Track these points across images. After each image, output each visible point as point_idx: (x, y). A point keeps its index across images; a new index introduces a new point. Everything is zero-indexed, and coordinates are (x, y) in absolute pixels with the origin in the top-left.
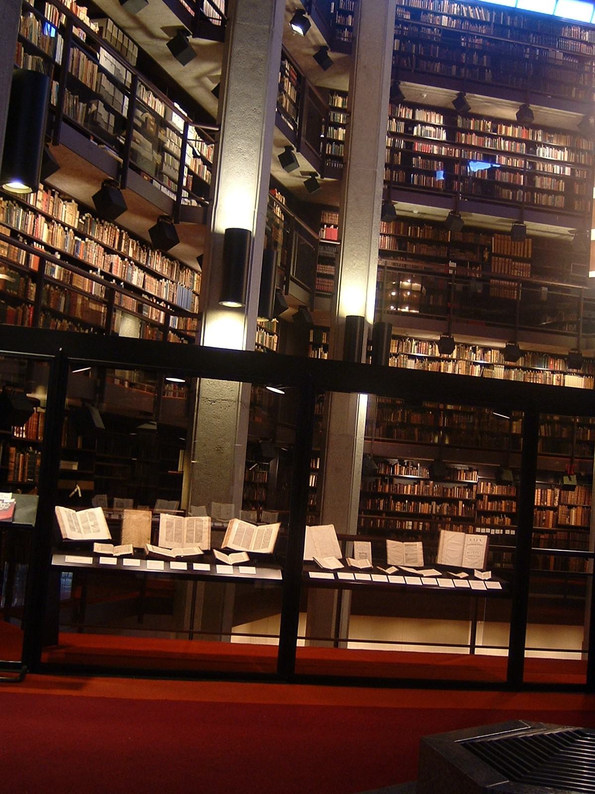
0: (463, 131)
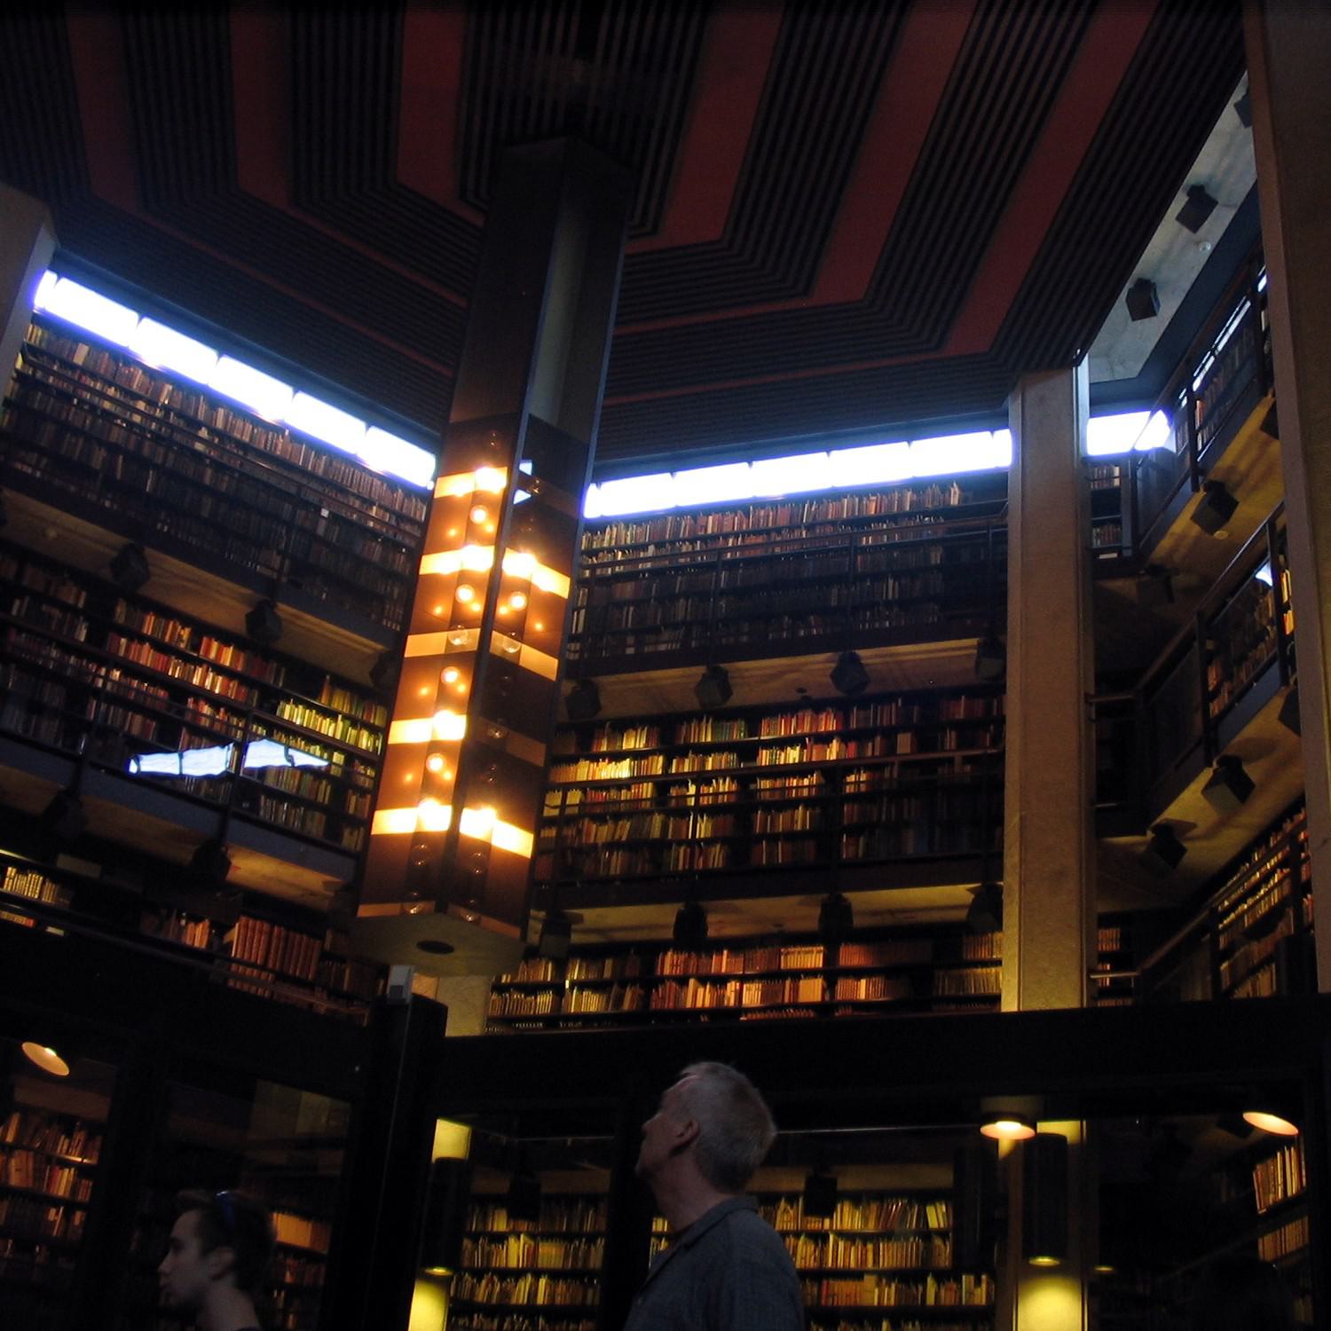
0: (122, 631)
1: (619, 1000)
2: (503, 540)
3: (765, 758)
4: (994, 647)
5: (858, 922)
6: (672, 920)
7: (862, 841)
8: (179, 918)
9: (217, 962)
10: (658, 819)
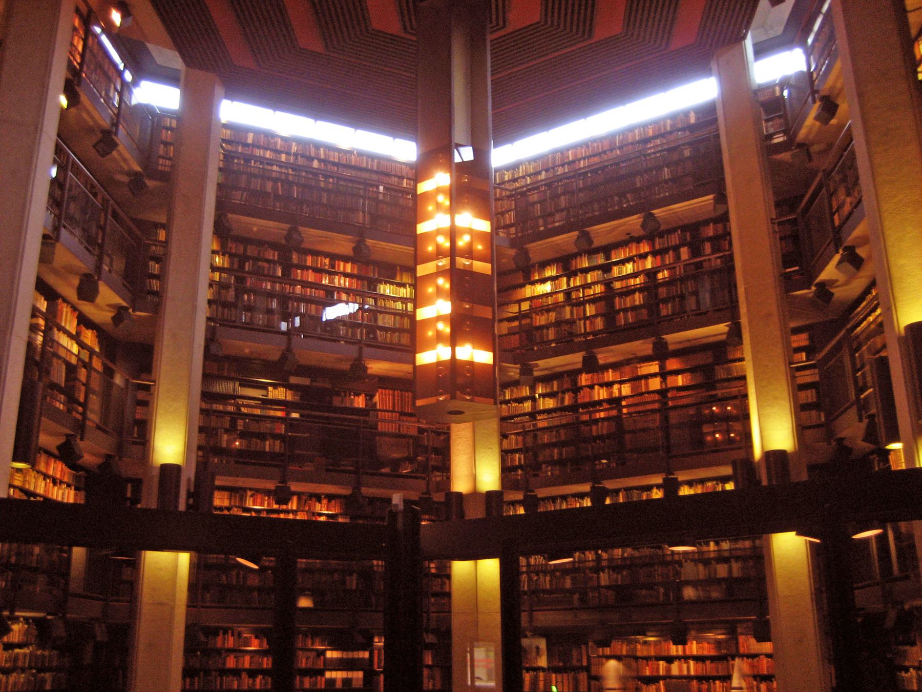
1: (563, 400)
2: (452, 210)
3: (616, 271)
4: (721, 198)
5: (671, 348)
6: (581, 359)
7: (670, 305)
8: (350, 395)
9: (371, 413)
10: (568, 309)
